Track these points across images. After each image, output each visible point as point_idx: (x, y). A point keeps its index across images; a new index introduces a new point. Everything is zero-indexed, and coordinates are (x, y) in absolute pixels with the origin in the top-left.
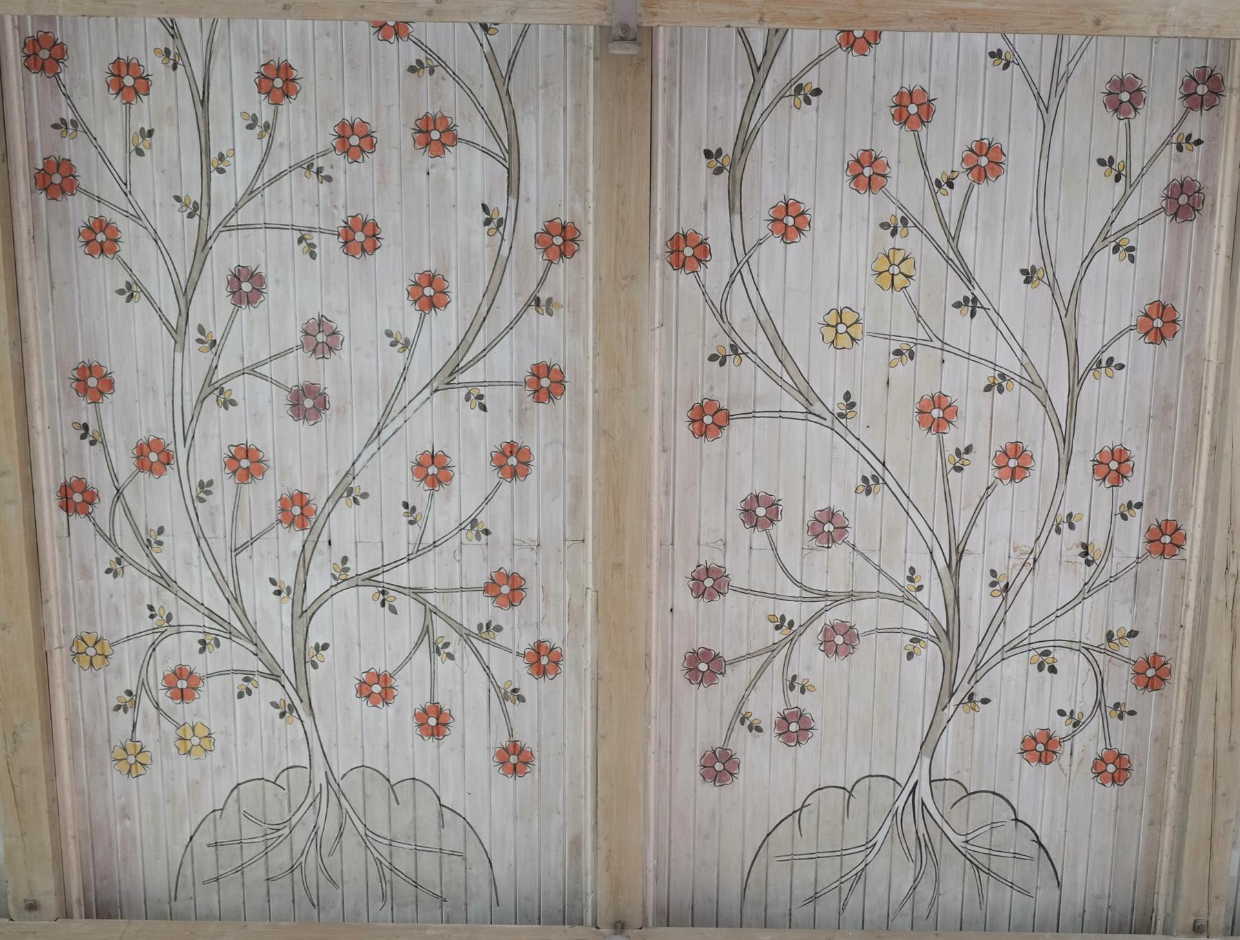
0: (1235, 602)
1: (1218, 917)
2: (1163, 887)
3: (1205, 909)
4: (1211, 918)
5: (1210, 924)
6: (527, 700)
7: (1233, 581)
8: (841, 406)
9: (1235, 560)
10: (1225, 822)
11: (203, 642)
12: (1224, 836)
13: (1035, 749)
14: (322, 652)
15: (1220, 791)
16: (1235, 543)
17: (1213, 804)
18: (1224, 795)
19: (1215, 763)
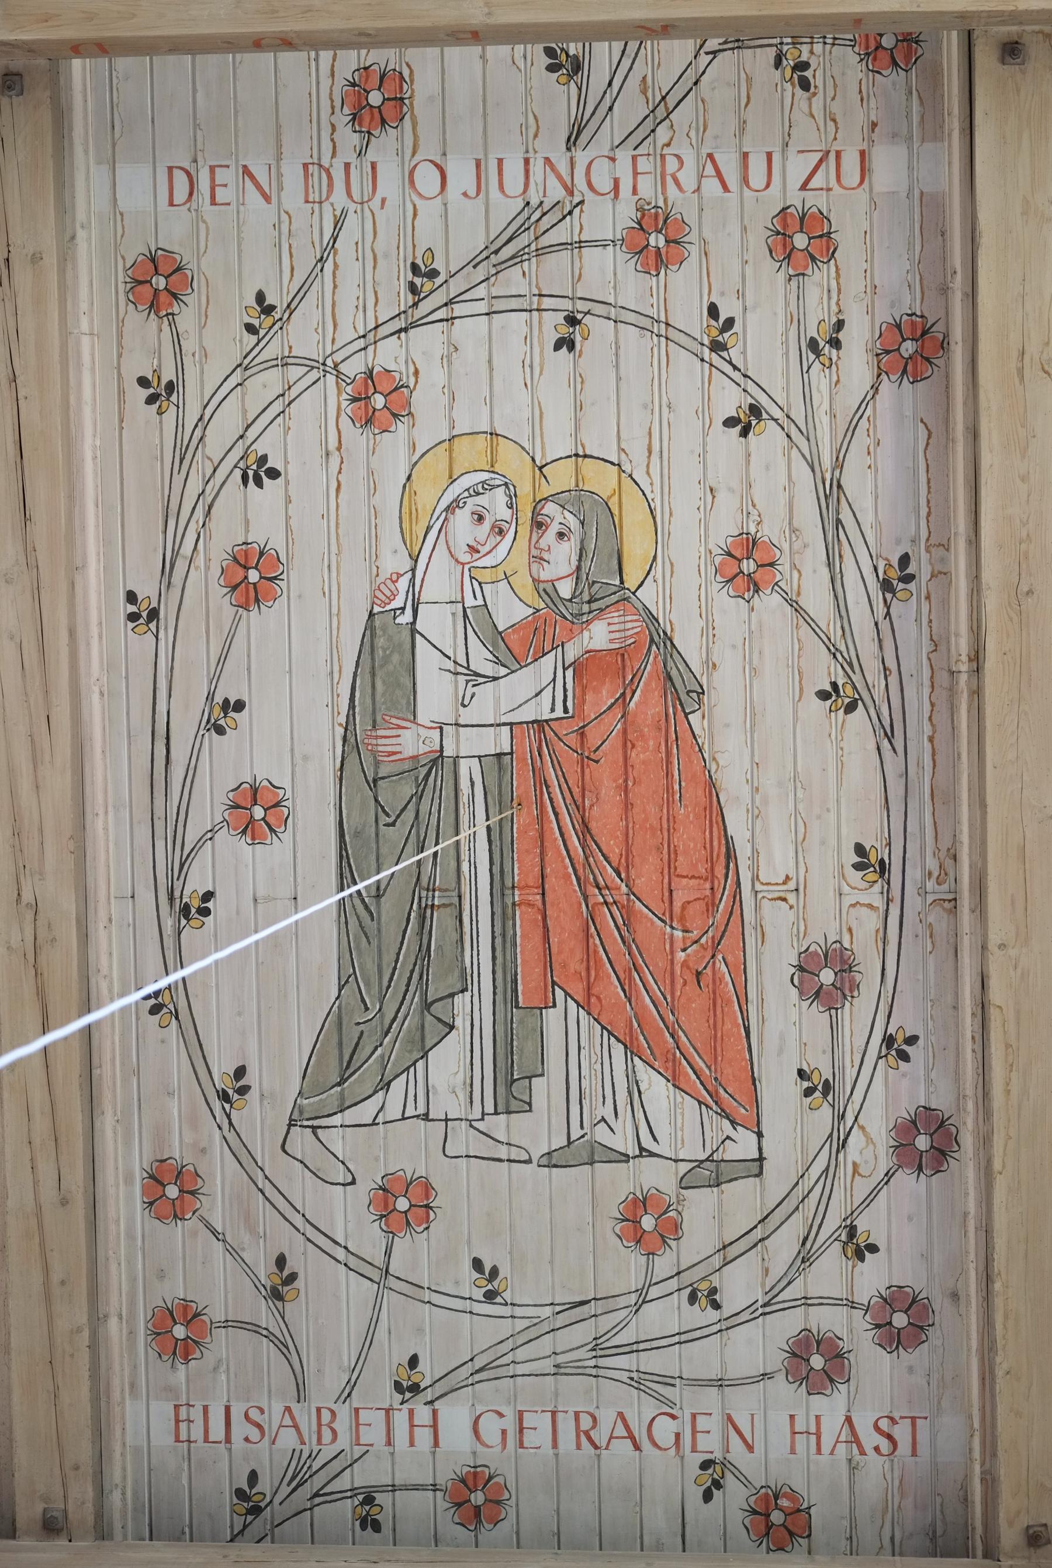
0: (38, 951)
1: (83, 1503)
2: (939, 1523)
3: (58, 1490)
4: (71, 1509)
5: (70, 1516)
6: (796, 1072)
7: (29, 916)
8: (251, 312)
9: (29, 883)
10: (72, 1332)
11: (268, 310)
12: (72, 1356)
13: (406, 1212)
14: (232, 714)
15: (56, 1277)
16: (25, 851)
17: (48, 1297)
18: (63, 1283)
19: (40, 1226)
